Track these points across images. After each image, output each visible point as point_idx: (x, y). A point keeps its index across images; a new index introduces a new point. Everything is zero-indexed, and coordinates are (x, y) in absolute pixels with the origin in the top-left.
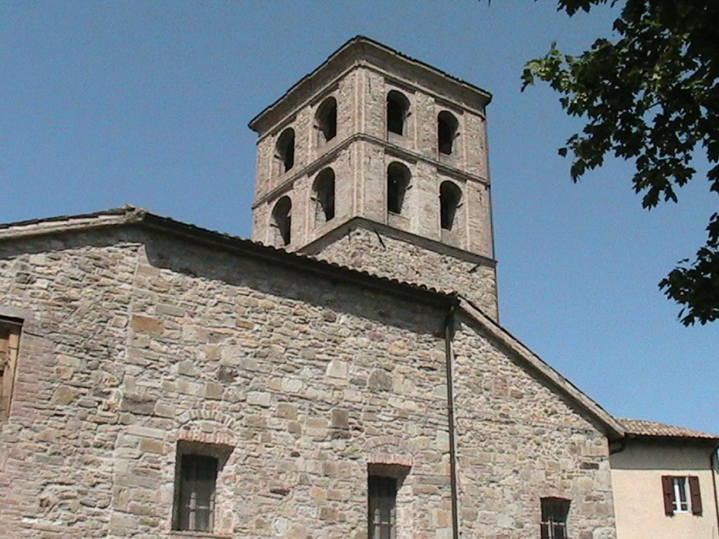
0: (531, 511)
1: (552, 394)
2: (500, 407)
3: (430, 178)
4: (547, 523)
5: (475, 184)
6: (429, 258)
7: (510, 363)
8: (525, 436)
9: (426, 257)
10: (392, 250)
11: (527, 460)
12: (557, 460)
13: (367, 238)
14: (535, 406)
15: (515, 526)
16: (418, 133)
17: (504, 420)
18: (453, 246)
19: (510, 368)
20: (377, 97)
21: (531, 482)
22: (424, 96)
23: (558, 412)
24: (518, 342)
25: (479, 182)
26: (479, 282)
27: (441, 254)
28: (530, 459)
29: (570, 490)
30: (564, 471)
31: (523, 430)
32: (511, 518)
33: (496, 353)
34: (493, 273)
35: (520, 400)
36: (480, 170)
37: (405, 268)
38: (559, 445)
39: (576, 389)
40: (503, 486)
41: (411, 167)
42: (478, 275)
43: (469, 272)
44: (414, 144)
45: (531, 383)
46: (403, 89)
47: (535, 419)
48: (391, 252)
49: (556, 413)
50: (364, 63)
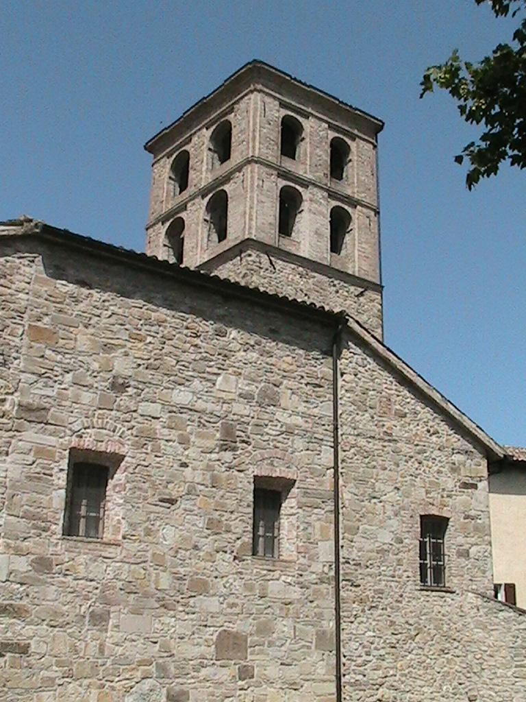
1: (435, 415)
5: (365, 210)
12: (437, 479)
14: (418, 425)
16: (311, 158)
24: (403, 362)
27: (330, 278)
30: (444, 490)
38: (439, 465)
40: (385, 502)
43: (357, 296)
44: (306, 168)
50: (259, 87)
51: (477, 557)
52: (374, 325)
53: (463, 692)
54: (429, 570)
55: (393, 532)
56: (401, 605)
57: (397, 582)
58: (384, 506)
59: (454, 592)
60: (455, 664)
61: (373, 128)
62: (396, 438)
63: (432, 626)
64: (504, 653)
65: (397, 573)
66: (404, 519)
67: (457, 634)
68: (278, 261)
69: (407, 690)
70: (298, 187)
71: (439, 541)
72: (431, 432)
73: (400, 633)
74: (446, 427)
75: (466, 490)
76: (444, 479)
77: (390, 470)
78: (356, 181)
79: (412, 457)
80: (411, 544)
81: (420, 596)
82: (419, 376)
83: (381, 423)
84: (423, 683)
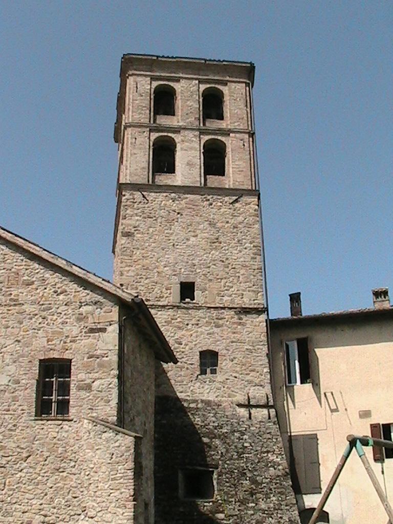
0: (29, 371)
1: (64, 278)
2: (11, 294)
3: (193, 140)
4: (52, 380)
5: (238, 135)
6: (189, 200)
7: (25, 260)
8: (31, 313)
9: (188, 200)
10: (154, 201)
11: (31, 331)
12: (62, 329)
13: (131, 197)
14: (46, 289)
15: (12, 383)
16: (182, 110)
17: (13, 303)
18: (220, 187)
19: (24, 263)
20: (143, 93)
21: (33, 348)
22: (189, 81)
23: (68, 290)
24: (30, 242)
25: (241, 132)
26: (242, 210)
27: (202, 195)
28: (33, 331)
29: (71, 351)
30: (67, 337)
31: (28, 308)
32: (8, 377)
33: (13, 255)
34: (256, 200)
35: (31, 286)
36: (243, 124)
37: (167, 212)
38: (65, 317)
39: (84, 270)
40: (5, 353)
41: (175, 137)
42: (241, 204)
43: (232, 203)
44: (178, 119)
45: (44, 272)
46: (215, 84)
47: (43, 299)
48: (154, 203)
49: (66, 292)
50: (130, 72)
51: (100, 389)
52: (251, 223)
53: (77, 504)
54: (53, 404)
55: (10, 376)
56: (13, 433)
57: (11, 414)
58: (3, 356)
59: (72, 420)
60: (72, 481)
61: (248, 72)
62: (22, 302)
63: (45, 449)
64: (104, 469)
65: (11, 408)
66: (22, 364)
67: (74, 455)
68: (151, 194)
69: (14, 502)
70: (170, 135)
71: (67, 379)
72: (59, 292)
73: (12, 456)
74: (76, 285)
75: (92, 335)
76: (68, 328)
77: (13, 328)
78: (228, 116)
79: (36, 315)
80: (27, 383)
81: (34, 425)
82: (44, 250)
83: (9, 293)
84: (32, 496)
